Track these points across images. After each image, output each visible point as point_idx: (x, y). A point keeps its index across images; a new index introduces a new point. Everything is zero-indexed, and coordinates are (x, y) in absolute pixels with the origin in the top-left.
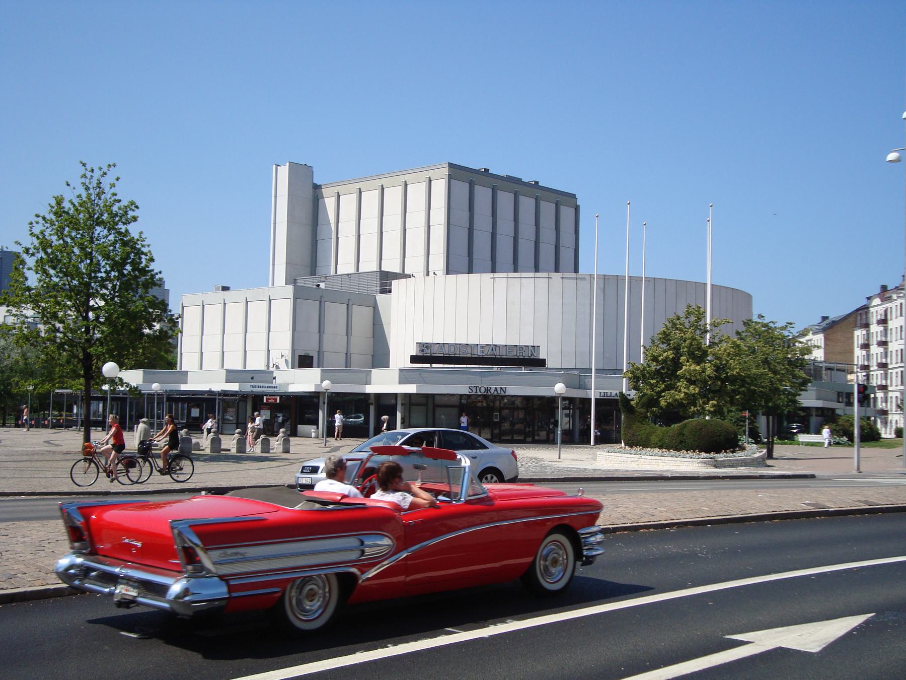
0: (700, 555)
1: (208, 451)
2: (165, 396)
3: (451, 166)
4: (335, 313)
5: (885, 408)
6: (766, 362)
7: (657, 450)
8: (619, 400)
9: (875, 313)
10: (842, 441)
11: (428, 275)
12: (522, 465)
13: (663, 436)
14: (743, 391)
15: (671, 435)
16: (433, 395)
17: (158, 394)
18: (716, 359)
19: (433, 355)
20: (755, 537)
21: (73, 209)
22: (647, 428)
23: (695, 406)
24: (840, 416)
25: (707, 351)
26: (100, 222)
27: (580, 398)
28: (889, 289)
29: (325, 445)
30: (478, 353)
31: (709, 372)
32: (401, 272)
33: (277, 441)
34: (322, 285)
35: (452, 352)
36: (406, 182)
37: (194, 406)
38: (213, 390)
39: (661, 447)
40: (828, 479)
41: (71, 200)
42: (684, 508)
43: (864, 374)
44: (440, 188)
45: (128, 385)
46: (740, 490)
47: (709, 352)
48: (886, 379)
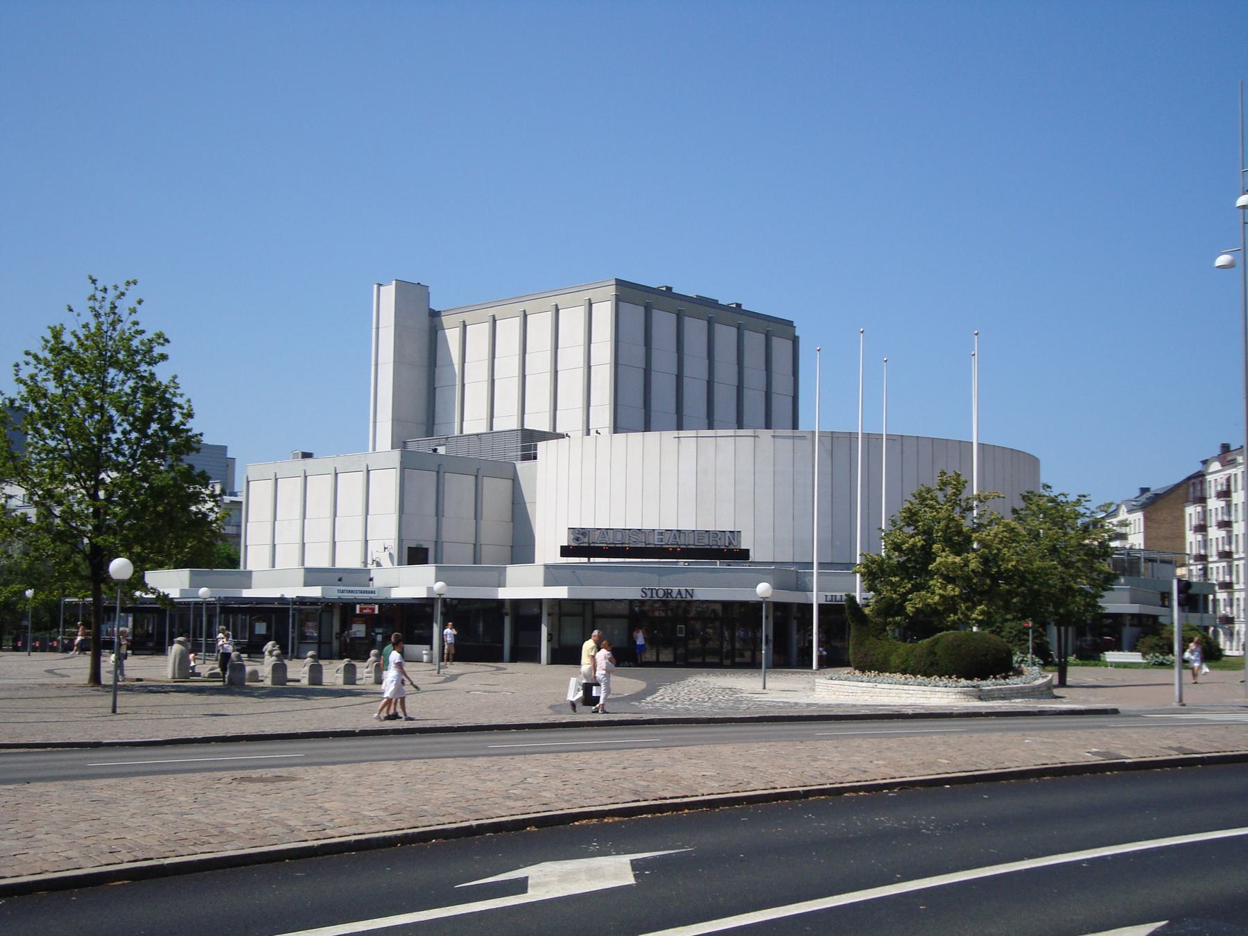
0: (924, 831)
1: (268, 682)
2: (218, 606)
3: (620, 283)
4: (459, 488)
5: (1229, 614)
6: (1054, 550)
7: (898, 676)
8: (846, 606)
9: (1213, 483)
10: (1168, 661)
11: (588, 433)
12: (710, 698)
13: (907, 655)
14: (1023, 592)
15: (918, 654)
16: (593, 601)
17: (208, 603)
18: (983, 548)
19: (592, 545)
20: (1069, 798)
21: (76, 344)
22: (885, 645)
23: (955, 614)
24: (1165, 625)
25: (972, 536)
26: (114, 362)
27: (799, 604)
28: (1232, 449)
29: (439, 673)
30: (655, 541)
31: (973, 565)
32: (552, 431)
33: (367, 668)
34: (442, 450)
35: (618, 541)
36: (556, 305)
37: (259, 620)
38: (286, 597)
39: (904, 672)
40: (1137, 715)
41: (75, 331)
42: (912, 760)
43: (1200, 567)
44: (604, 313)
45: (154, 591)
46: (1000, 734)
47: (973, 538)
48: (1230, 574)
